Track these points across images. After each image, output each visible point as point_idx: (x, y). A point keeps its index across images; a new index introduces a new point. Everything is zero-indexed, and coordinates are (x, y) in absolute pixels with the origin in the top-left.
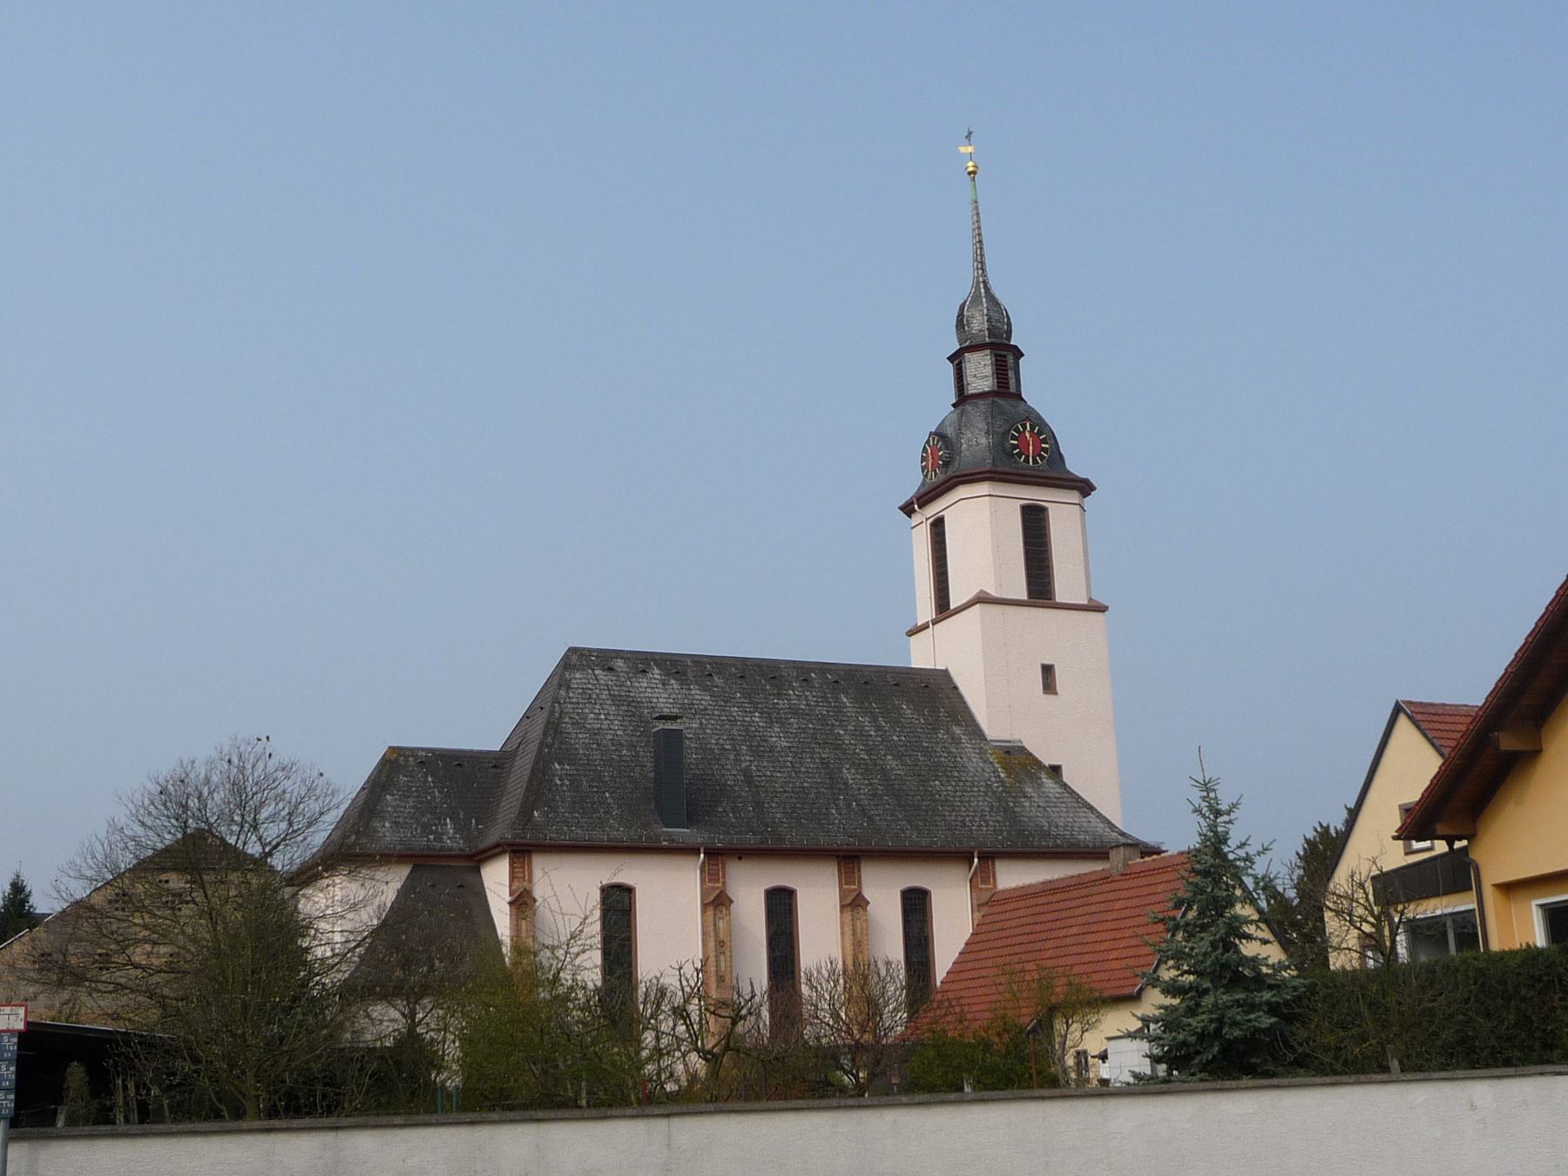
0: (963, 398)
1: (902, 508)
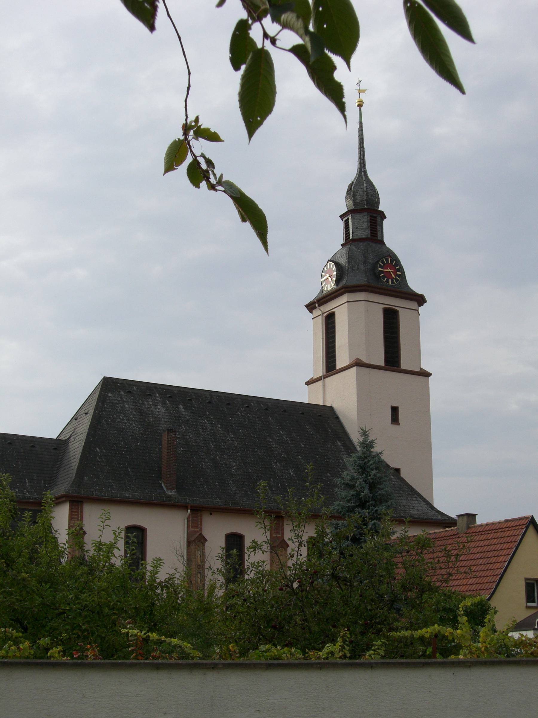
1: (307, 306)
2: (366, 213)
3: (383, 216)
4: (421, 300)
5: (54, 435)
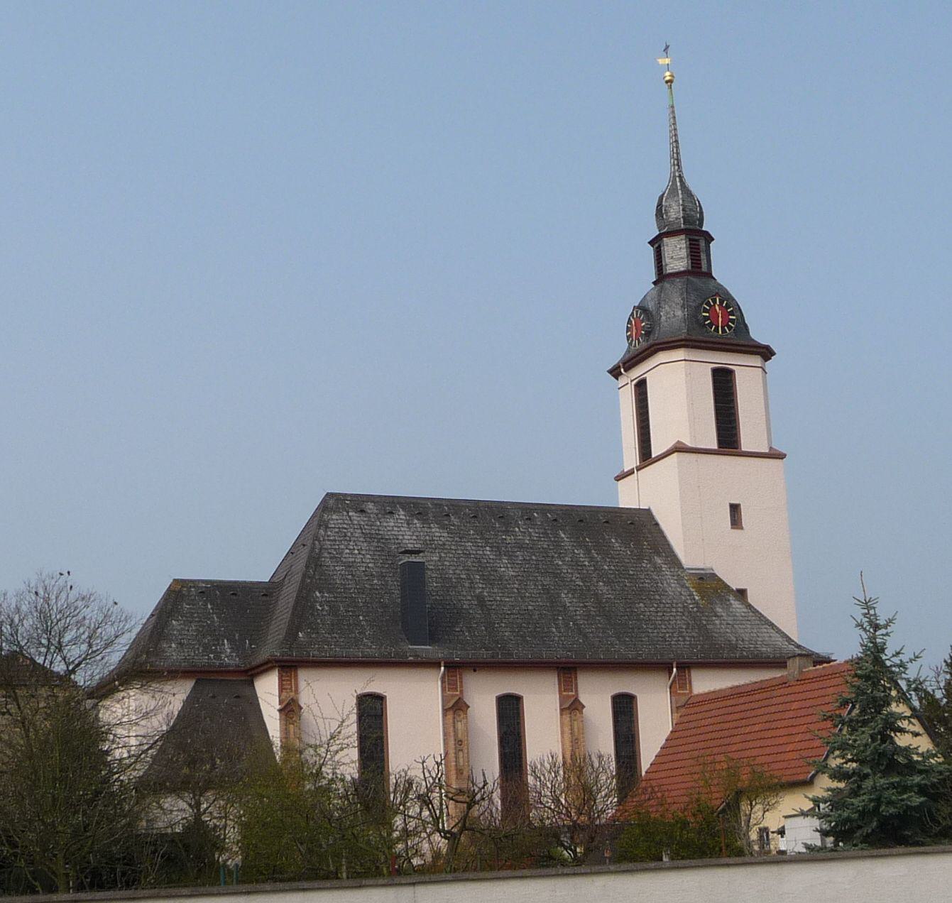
0: (662, 276)
2: (683, 237)
3: (709, 238)
4: (766, 353)
5: (266, 578)
